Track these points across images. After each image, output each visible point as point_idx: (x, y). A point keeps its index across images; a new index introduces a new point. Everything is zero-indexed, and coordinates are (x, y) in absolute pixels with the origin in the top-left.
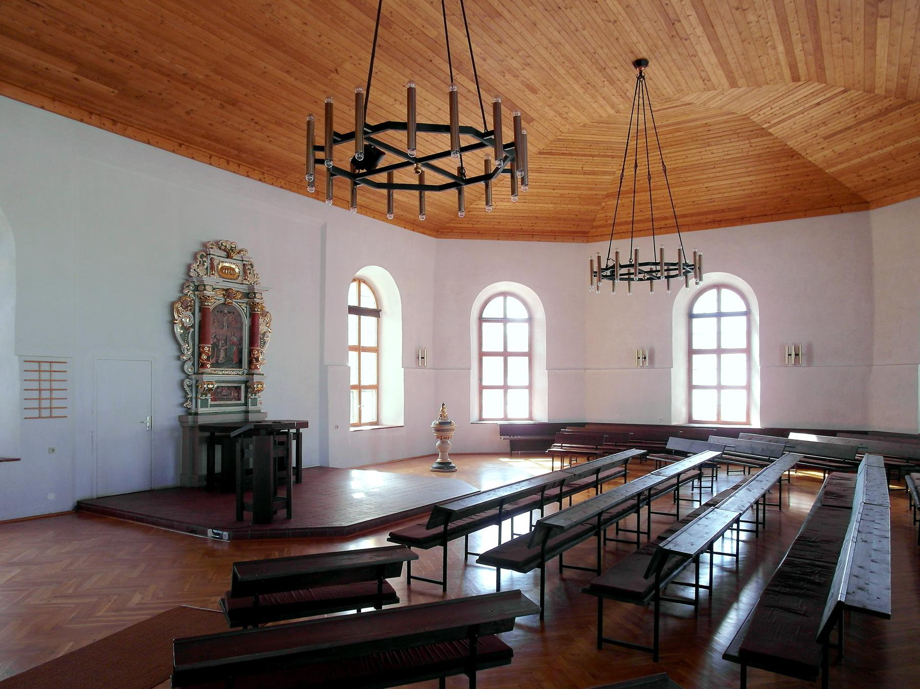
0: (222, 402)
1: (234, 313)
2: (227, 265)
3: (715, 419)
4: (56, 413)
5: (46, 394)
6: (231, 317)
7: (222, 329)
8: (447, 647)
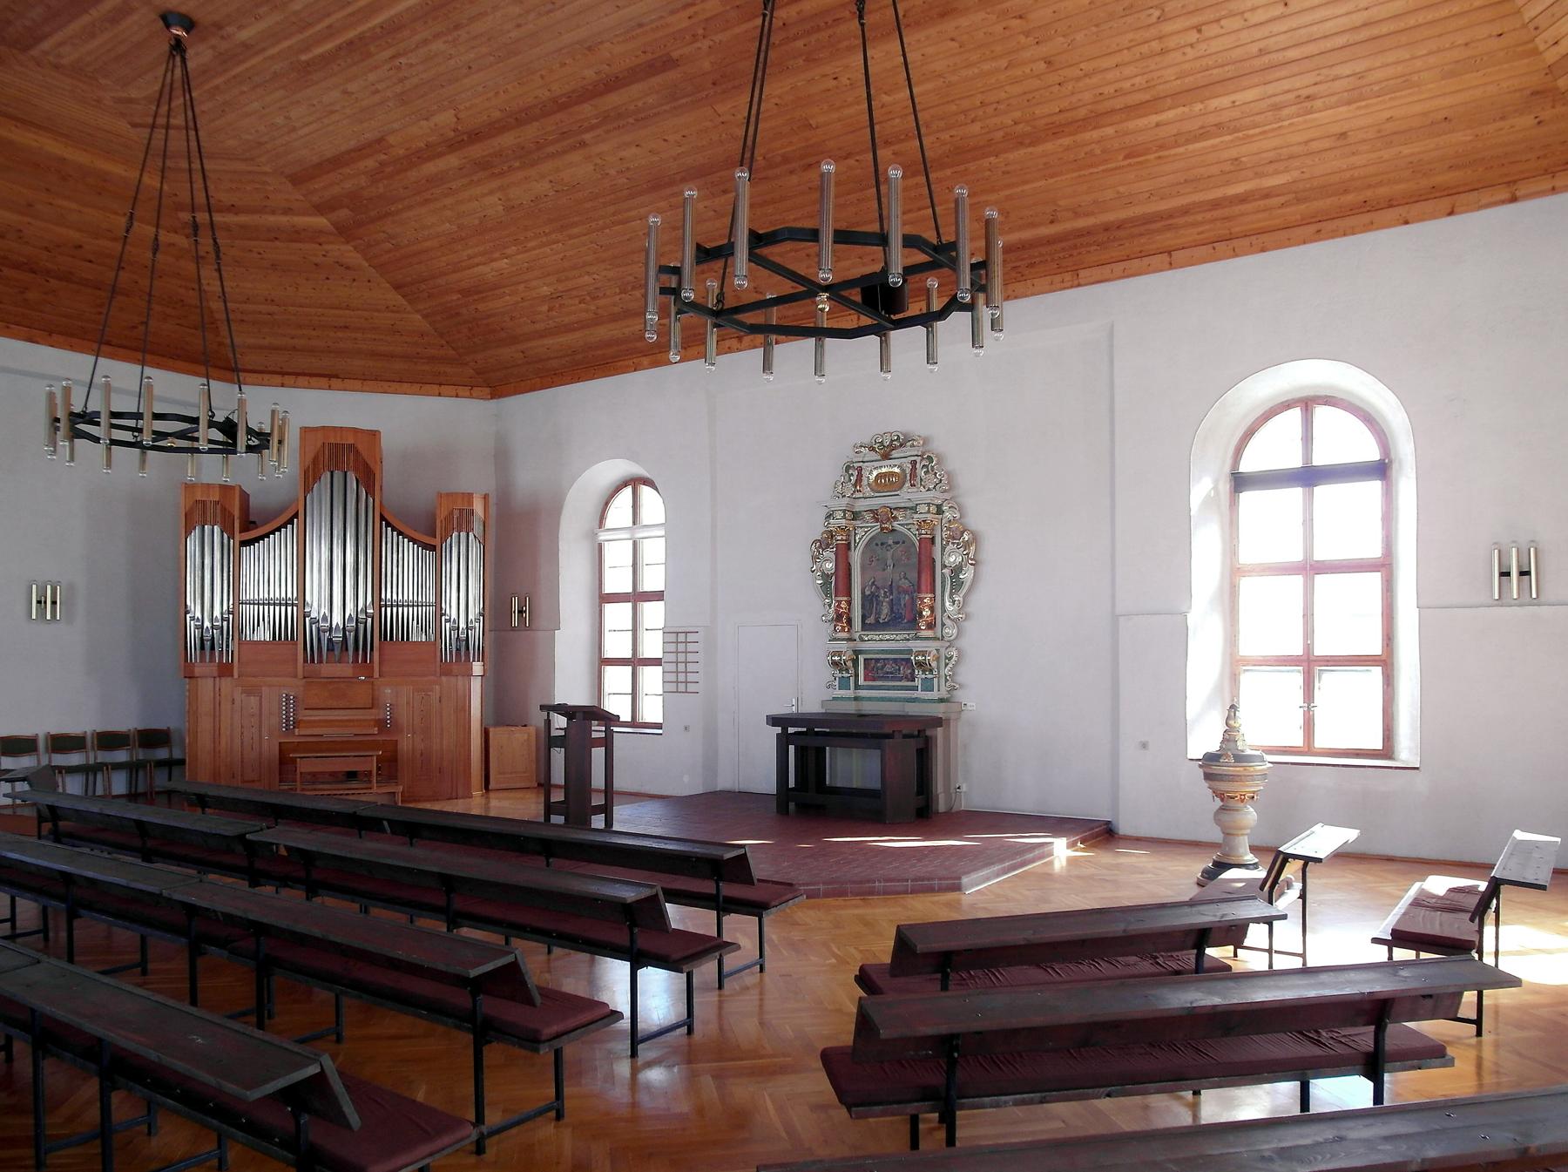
0: (886, 683)
1: (904, 542)
2: (884, 470)
3: (1298, 740)
4: (691, 688)
5: (681, 667)
6: (900, 548)
7: (884, 570)
8: (733, 1060)
